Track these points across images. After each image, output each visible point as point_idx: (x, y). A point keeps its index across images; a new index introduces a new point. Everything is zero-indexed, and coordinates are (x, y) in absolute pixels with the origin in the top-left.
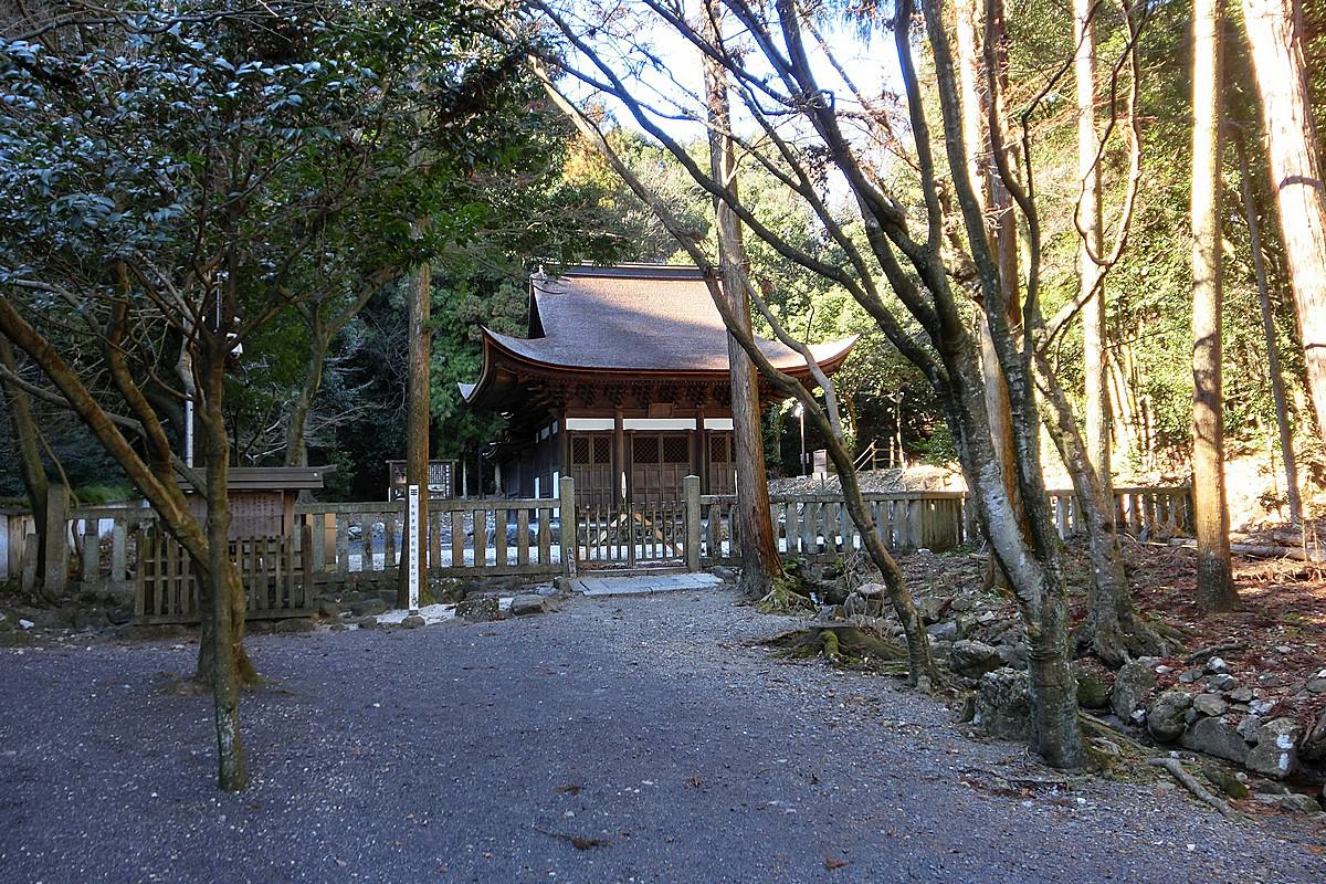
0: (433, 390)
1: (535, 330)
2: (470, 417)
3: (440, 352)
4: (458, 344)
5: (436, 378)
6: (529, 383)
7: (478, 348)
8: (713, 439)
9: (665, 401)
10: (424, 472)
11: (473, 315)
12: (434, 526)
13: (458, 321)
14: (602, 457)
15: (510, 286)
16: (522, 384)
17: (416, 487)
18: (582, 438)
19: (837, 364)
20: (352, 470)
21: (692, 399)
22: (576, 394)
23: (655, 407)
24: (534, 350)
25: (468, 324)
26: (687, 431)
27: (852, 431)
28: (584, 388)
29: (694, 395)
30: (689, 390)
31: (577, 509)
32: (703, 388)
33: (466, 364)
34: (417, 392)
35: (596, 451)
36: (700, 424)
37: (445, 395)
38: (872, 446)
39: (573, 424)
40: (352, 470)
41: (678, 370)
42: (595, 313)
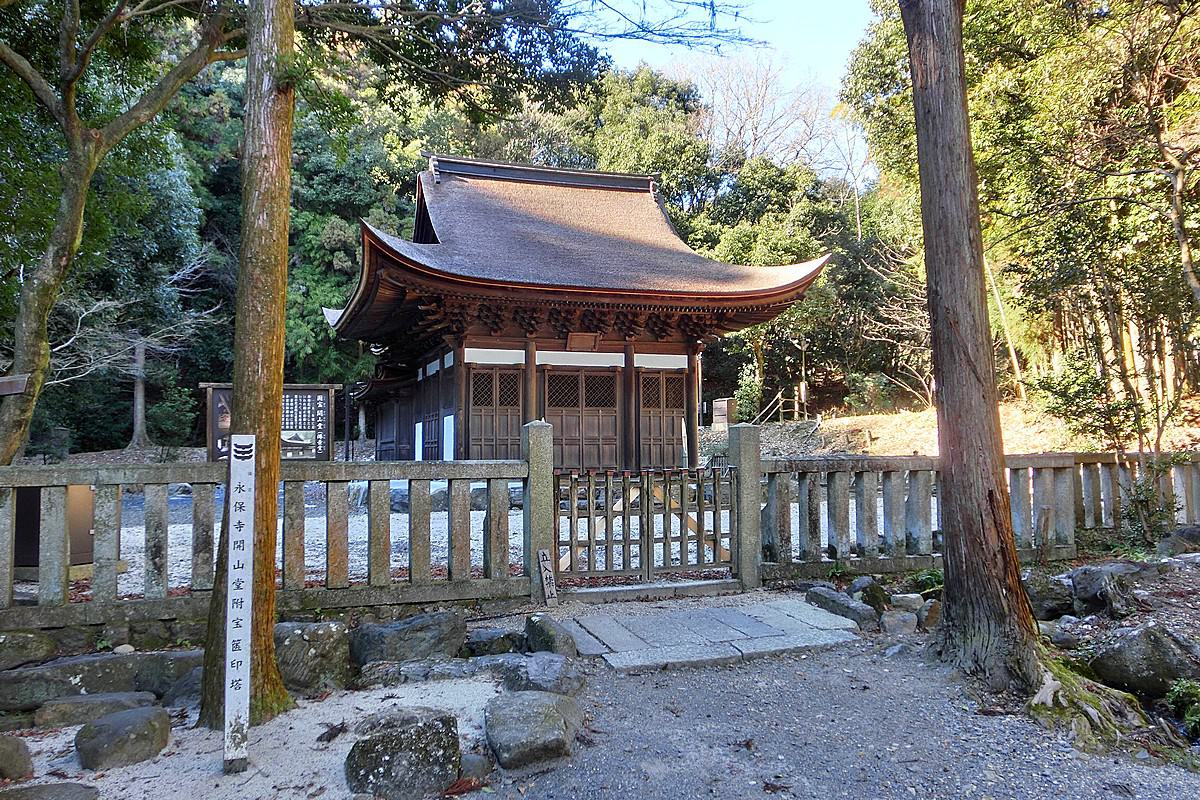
0: (292, 323)
1: (424, 233)
2: (334, 354)
3: (301, 281)
4: (320, 273)
5: (294, 310)
6: (419, 300)
7: (344, 279)
8: (645, 380)
9: (588, 330)
10: (271, 403)
11: (340, 240)
12: (292, 511)
13: (322, 247)
14: (510, 397)
15: (381, 210)
16: (410, 301)
17: (248, 439)
18: (483, 376)
19: (800, 291)
20: (192, 410)
21: (620, 329)
22: (479, 317)
23: (576, 337)
24: (429, 256)
25: (332, 251)
26: (613, 369)
27: (757, 379)
28: (489, 309)
29: (623, 323)
30: (618, 318)
31: (557, 479)
32: (636, 315)
33: (331, 295)
34: (261, 222)
35: (501, 390)
36: (629, 360)
37: (305, 329)
38: (779, 395)
39: (473, 355)
40: (192, 410)
41: (613, 290)
42: (500, 219)
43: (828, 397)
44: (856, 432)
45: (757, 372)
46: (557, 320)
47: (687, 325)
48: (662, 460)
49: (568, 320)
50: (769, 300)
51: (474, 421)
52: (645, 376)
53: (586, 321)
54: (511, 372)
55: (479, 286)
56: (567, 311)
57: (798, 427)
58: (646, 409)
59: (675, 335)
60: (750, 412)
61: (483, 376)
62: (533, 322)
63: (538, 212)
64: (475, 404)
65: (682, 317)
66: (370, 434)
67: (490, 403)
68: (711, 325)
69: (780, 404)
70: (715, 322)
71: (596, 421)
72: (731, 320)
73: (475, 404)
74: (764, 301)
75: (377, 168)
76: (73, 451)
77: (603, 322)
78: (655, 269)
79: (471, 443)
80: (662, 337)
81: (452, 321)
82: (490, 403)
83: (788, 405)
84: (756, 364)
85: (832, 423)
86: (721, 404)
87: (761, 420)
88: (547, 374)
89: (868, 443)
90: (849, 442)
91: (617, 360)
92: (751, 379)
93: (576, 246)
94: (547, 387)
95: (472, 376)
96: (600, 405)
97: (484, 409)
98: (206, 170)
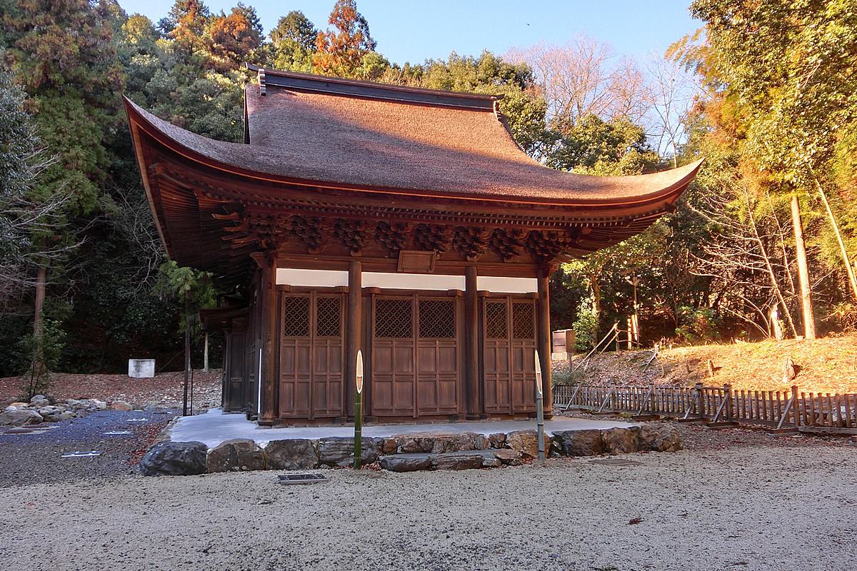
8: (489, 306)
9: (423, 247)
18: (299, 299)
19: (669, 200)
21: (461, 248)
22: (293, 232)
23: (408, 256)
26: (453, 293)
28: (305, 222)
30: (457, 234)
32: (478, 231)
36: (471, 283)
38: (615, 327)
43: (656, 329)
44: (694, 362)
45: (594, 305)
46: (386, 236)
47: (536, 243)
48: (510, 399)
49: (399, 236)
50: (636, 211)
51: (286, 354)
52: (489, 301)
53: (421, 238)
54: (332, 296)
55: (260, 182)
56: (398, 225)
57: (635, 356)
58: (490, 339)
59: (523, 256)
60: (588, 343)
61: (297, 301)
62: (357, 238)
63: (371, 124)
64: (288, 332)
65: (531, 235)
66: (216, 362)
67: (305, 332)
68: (564, 244)
69: (616, 335)
70: (569, 240)
71: (432, 354)
72: (587, 237)
73: (288, 332)
74: (628, 212)
75: (136, 42)
76: (63, 368)
77: (439, 238)
78: (499, 177)
79: (282, 380)
80: (509, 257)
81: (259, 235)
82: (305, 332)
83: (623, 336)
84: (593, 298)
85: (668, 353)
86: (561, 334)
87: (600, 349)
88: (374, 299)
89: (711, 373)
90: (690, 372)
91: (457, 283)
92: (589, 311)
93: (407, 154)
94: (374, 314)
95: (284, 300)
96: (296, 333)
97: (498, 341)
98: (107, 132)
